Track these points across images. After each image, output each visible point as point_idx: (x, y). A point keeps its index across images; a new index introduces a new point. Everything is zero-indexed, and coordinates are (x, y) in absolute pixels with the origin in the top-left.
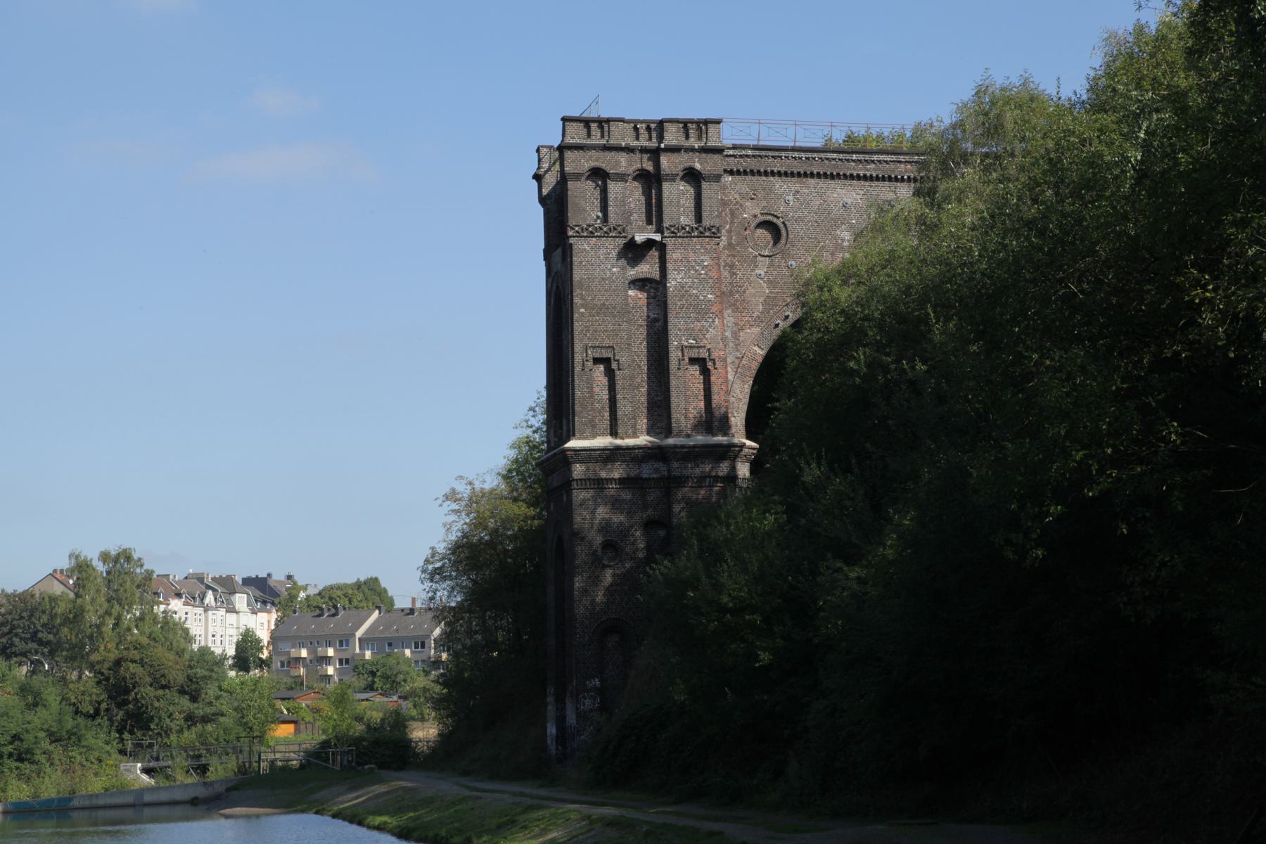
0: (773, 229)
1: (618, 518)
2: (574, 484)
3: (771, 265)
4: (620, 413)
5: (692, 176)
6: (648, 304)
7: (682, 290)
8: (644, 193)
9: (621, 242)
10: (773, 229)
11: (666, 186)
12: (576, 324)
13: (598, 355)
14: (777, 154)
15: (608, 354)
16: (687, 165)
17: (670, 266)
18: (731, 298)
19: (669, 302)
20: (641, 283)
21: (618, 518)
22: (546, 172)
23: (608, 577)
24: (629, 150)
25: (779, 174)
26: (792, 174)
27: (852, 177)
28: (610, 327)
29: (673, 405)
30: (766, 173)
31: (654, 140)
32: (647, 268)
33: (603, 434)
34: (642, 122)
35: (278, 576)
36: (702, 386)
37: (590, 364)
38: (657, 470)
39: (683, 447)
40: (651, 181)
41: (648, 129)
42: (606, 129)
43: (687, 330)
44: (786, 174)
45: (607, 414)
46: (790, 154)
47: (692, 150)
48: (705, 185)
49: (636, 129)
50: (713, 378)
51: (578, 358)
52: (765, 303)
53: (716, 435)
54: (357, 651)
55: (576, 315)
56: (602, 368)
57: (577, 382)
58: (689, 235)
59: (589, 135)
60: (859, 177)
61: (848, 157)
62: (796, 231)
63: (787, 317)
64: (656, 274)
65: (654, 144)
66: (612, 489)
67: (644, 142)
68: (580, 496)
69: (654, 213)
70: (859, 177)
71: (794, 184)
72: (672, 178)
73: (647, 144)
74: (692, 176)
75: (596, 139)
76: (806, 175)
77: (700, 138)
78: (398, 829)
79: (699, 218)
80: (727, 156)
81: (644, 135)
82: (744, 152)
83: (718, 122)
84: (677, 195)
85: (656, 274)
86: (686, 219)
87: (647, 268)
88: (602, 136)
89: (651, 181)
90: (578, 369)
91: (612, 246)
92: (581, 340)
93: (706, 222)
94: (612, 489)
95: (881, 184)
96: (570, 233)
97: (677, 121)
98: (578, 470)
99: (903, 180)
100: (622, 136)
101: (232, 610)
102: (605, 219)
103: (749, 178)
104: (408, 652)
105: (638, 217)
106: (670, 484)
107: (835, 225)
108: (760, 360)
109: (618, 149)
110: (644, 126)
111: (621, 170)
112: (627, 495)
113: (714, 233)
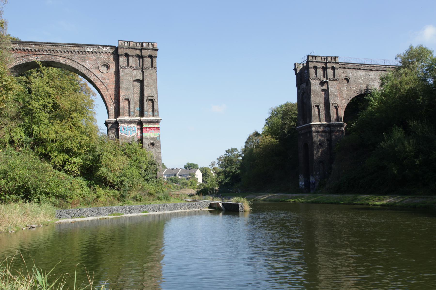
0: (347, 80)
1: (322, 139)
2: (313, 132)
3: (347, 87)
4: (321, 117)
5: (333, 68)
6: (324, 95)
8: (323, 72)
9: (320, 81)
10: (347, 80)
11: (328, 70)
12: (312, 98)
13: (316, 105)
14: (348, 64)
15: (318, 105)
16: (332, 66)
17: (329, 87)
18: (341, 94)
19: (329, 94)
20: (323, 90)
21: (322, 139)
22: (297, 68)
23: (321, 151)
24: (321, 62)
25: (348, 68)
26: (351, 68)
27: (362, 69)
28: (318, 99)
29: (331, 115)
30: (346, 68)
31: (325, 60)
32: (325, 87)
33: (317, 121)
34: (323, 57)
36: (336, 112)
37: (315, 107)
38: (328, 129)
39: (334, 124)
40: (325, 69)
41: (324, 58)
42: (316, 58)
43: (333, 100)
44: (350, 68)
45: (318, 117)
46: (351, 64)
47: (333, 63)
48: (335, 70)
49: (322, 58)
50: (338, 110)
51: (312, 105)
52: (346, 95)
53: (340, 122)
54: (163, 176)
55: (312, 97)
56: (317, 108)
57: (312, 110)
58: (333, 80)
59: (313, 59)
60: (363, 69)
61: (361, 65)
62: (352, 80)
63: (351, 98)
64: (326, 88)
65: (325, 61)
66: (321, 133)
67: (323, 61)
68: (314, 134)
69: (326, 76)
70: (363, 69)
71: (351, 70)
72: (329, 68)
73: (324, 61)
74: (333, 68)
75: (314, 60)
76: (353, 69)
77: (334, 60)
79: (334, 76)
80: (340, 64)
81: (323, 60)
82: (342, 64)
83: (338, 57)
84: (330, 72)
85: (326, 88)
86: (332, 77)
87: (325, 87)
88: (316, 59)
89: (325, 69)
90: (312, 108)
91: (318, 82)
92: (313, 102)
93: (336, 78)
94: (321, 133)
95: (367, 71)
96: (310, 79)
97: (330, 57)
98: (314, 129)
99: (371, 70)
100: (319, 59)
102: (316, 77)
103: (343, 69)
104: (173, 176)
106: (331, 132)
107: (359, 79)
108: (346, 107)
109: (319, 62)
110: (323, 58)
111: (320, 66)
112: (324, 134)
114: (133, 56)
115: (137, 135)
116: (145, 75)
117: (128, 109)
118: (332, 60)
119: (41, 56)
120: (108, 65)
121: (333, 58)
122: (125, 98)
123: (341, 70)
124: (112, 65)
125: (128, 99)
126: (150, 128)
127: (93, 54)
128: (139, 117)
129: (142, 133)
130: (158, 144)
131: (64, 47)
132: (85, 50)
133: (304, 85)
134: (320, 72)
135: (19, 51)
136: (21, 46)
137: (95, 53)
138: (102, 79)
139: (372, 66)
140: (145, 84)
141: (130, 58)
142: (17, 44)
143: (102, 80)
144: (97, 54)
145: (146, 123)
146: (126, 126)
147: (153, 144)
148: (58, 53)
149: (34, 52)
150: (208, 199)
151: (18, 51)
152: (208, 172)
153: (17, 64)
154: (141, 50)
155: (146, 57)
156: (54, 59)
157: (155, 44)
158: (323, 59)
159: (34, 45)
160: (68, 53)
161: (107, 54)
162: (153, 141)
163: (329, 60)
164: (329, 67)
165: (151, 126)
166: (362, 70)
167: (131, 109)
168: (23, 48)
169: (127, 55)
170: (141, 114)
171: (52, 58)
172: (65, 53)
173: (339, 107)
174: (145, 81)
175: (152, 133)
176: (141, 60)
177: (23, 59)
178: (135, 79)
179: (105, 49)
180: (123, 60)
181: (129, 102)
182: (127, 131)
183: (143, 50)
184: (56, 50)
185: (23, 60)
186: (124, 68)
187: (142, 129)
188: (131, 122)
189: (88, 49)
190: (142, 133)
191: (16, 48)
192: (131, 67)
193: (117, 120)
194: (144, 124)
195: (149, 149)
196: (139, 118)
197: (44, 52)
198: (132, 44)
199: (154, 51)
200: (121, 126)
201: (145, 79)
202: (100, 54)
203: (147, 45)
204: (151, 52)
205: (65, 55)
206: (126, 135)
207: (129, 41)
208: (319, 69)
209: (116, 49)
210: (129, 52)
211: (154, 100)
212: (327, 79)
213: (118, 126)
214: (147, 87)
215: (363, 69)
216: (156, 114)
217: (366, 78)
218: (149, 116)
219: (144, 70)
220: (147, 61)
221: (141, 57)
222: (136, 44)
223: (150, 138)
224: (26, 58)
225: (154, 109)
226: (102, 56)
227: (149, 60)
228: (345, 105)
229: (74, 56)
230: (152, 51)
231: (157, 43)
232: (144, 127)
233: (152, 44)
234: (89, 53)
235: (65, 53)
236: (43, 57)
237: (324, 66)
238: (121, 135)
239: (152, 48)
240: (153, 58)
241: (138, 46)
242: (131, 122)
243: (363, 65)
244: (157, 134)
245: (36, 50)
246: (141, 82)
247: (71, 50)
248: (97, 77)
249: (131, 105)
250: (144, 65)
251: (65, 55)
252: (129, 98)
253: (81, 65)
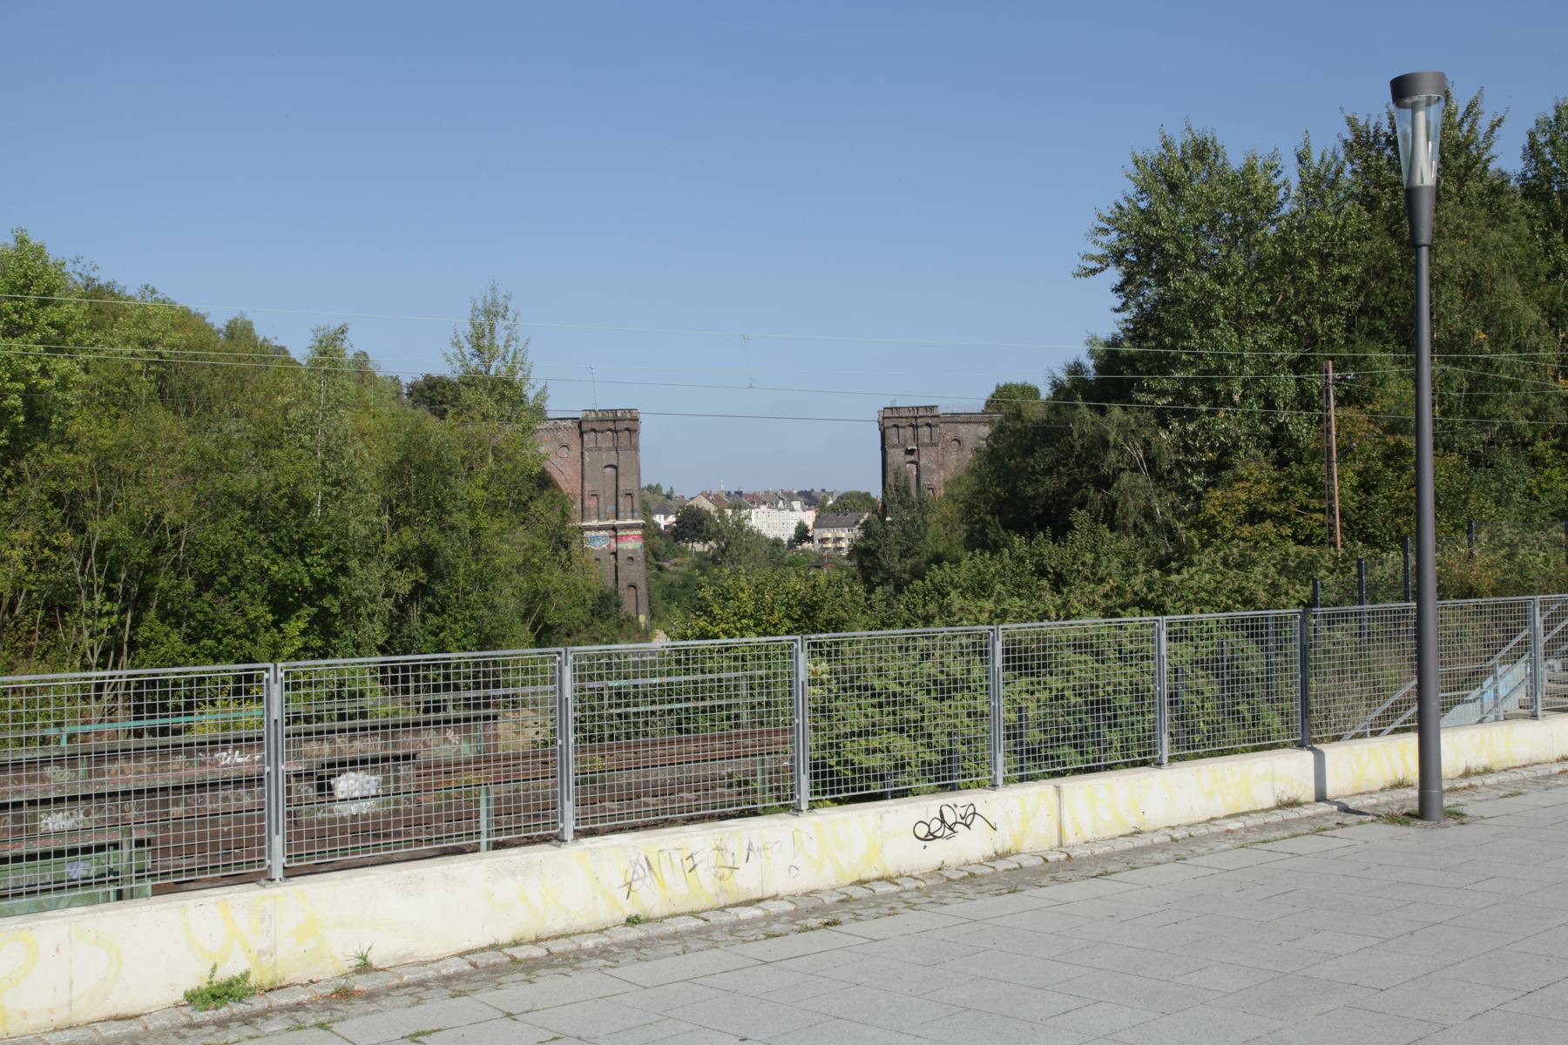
7: (925, 466)
35: (817, 490)
69: (916, 438)
71: (965, 426)
75: (895, 414)
78: (1038, 861)
86: (927, 441)
101: (792, 510)
105: (910, 441)
113: (936, 445)
146: (593, 533)
150: (1454, 458)
152: (475, 309)
165: (628, 533)
179: (563, 423)
186: (590, 450)
218: (625, 519)
223: (628, 551)
226: (560, 434)
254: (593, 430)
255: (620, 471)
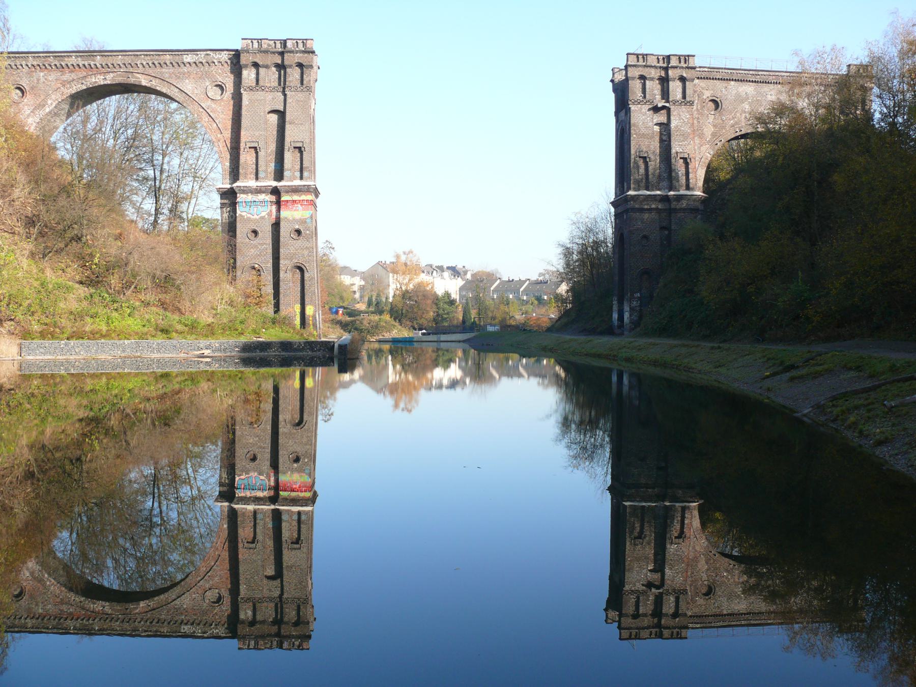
0: (716, 104)
3: (715, 118)
5: (683, 79)
10: (716, 104)
12: (632, 142)
17: (672, 118)
18: (697, 132)
40: (664, 81)
41: (664, 59)
46: (723, 70)
47: (682, 68)
48: (687, 83)
49: (658, 59)
50: (690, 166)
55: (632, 138)
59: (638, 61)
62: (260, 234)
65: (665, 65)
67: (661, 64)
69: (665, 94)
71: (724, 84)
72: (674, 80)
75: (641, 63)
77: (685, 63)
81: (661, 62)
83: (694, 56)
84: (675, 88)
86: (679, 96)
88: (644, 62)
89: (664, 81)
96: (630, 103)
97: (676, 55)
100: (652, 61)
101: (443, 278)
102: (645, 97)
105: (658, 97)
109: (651, 66)
110: (662, 57)
113: (691, 103)
114: (267, 67)
115: (270, 214)
116: (289, 100)
117: (254, 166)
118: (680, 62)
119: (112, 75)
120: (223, 85)
121: (683, 58)
122: (249, 145)
123: (703, 83)
124: (229, 81)
125: (255, 148)
126: (294, 202)
127: (197, 65)
128: (275, 180)
129: (279, 210)
130: (308, 232)
131: (148, 58)
132: (183, 59)
133: (622, 113)
134: (654, 88)
135: (77, 68)
136: (79, 59)
137: (200, 65)
138: (211, 112)
139: (771, 73)
140: (288, 117)
141: (262, 71)
142: (74, 57)
143: (211, 114)
144: (203, 65)
145: (287, 192)
146: (250, 197)
147: (298, 232)
148: (138, 67)
149: (101, 69)
151: (74, 68)
153: (73, 92)
154: (282, 54)
155: (290, 66)
156: (132, 80)
157: (309, 42)
158: (660, 60)
159: (100, 56)
160: (156, 67)
161: (222, 65)
162: (299, 225)
163: (674, 62)
164: (672, 77)
165: (296, 197)
166: (751, 83)
167: (259, 166)
168: (83, 63)
169: (256, 65)
170: (279, 175)
171: (129, 78)
172: (150, 67)
173: (692, 160)
174: (287, 114)
175: (298, 210)
176: (282, 72)
177: (83, 82)
178: (269, 110)
180: (248, 75)
181: (257, 153)
182: (252, 207)
183: (286, 55)
184: (136, 62)
185: (82, 84)
186: (251, 89)
187: (278, 203)
188: (258, 191)
189: (188, 58)
190: (279, 210)
191: (71, 63)
192: (263, 88)
193: (232, 188)
194: (282, 194)
195: (291, 241)
196: (275, 184)
197: (115, 67)
198: (265, 44)
199: (306, 55)
200: (241, 197)
201: (287, 110)
202: (209, 65)
203: (293, 44)
204: (299, 58)
205: (150, 71)
206: (249, 215)
207: (261, 40)
208: (652, 82)
209: (236, 56)
210: (259, 59)
211: (303, 149)
212: (668, 101)
213: (236, 198)
214: (290, 124)
215: (751, 80)
216: (305, 174)
217: (758, 100)
218: (292, 178)
219: (286, 93)
220: (294, 74)
221: (281, 67)
222: (275, 43)
223: (295, 220)
224: (87, 80)
225: (304, 166)
227: (298, 70)
228: (709, 155)
229: (166, 72)
230: (302, 55)
231: (312, 40)
232: (283, 199)
233: (304, 42)
234: (190, 65)
235: (150, 67)
236: (114, 76)
237: (663, 74)
238: (240, 215)
239: (303, 49)
240: (305, 69)
241: (277, 46)
242: (258, 191)
243: (751, 72)
244: (308, 212)
245: (104, 64)
246: (282, 114)
247: (160, 61)
248: (203, 108)
249: (259, 158)
250: (287, 83)
251: (150, 71)
252: (257, 146)
253: (177, 87)
254: (256, 65)
255: (288, 118)
